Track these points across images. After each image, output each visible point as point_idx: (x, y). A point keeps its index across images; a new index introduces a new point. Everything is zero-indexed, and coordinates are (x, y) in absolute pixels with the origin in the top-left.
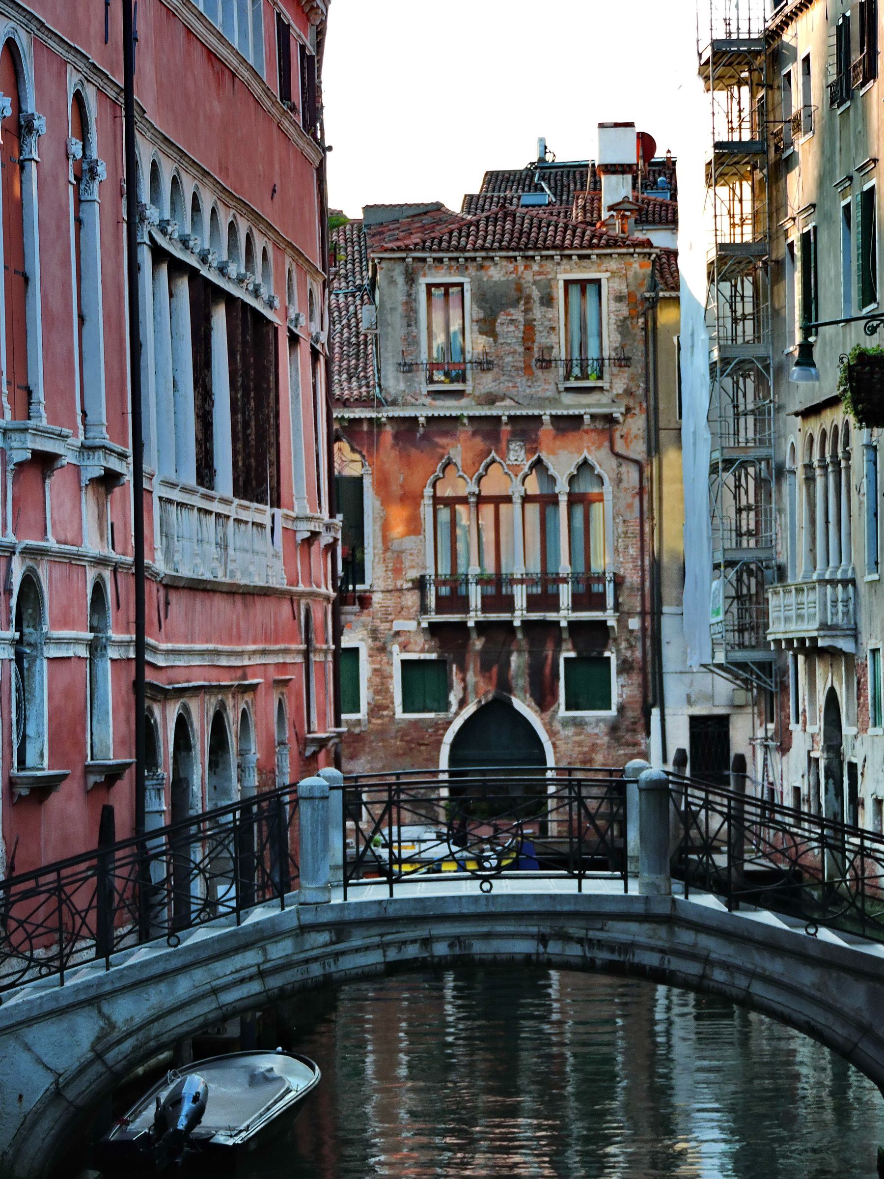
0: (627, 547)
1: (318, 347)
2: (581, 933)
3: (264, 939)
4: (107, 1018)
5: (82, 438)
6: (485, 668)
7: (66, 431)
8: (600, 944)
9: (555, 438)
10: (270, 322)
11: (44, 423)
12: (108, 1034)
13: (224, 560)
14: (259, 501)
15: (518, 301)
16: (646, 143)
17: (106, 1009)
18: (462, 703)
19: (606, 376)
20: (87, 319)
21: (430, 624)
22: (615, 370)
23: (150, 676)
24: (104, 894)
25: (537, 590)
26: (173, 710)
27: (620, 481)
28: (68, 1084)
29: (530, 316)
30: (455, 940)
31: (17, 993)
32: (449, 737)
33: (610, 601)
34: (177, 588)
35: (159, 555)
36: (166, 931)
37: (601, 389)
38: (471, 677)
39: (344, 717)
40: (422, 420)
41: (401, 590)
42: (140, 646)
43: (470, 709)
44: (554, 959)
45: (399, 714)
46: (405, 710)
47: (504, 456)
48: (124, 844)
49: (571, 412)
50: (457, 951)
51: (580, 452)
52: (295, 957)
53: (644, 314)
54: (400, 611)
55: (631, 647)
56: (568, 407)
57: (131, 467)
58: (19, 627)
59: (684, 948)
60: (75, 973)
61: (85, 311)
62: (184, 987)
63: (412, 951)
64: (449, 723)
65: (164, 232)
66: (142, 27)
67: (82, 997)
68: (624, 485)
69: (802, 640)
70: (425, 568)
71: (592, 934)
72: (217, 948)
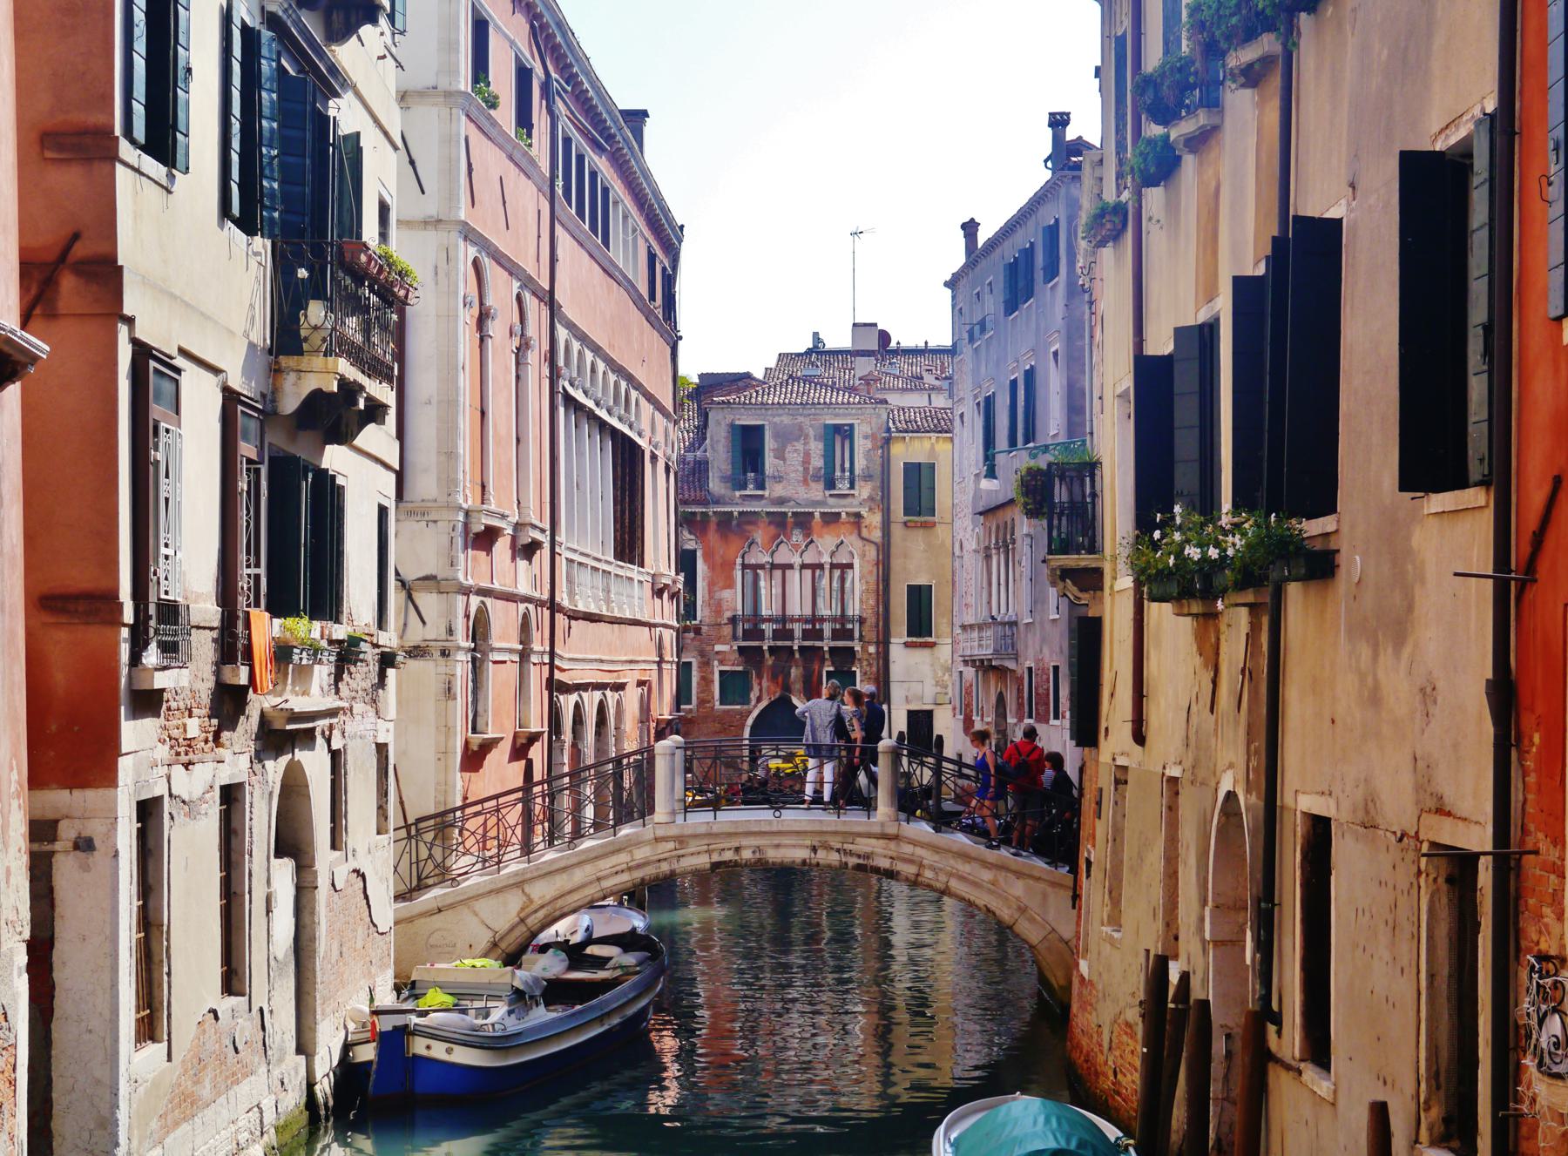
0: (868, 599)
1: (670, 464)
2: (839, 846)
3: (631, 845)
4: (528, 896)
5: (517, 518)
6: (774, 678)
7: (507, 513)
8: (851, 853)
9: (822, 527)
10: (639, 446)
11: (493, 507)
12: (527, 907)
13: (608, 601)
14: (630, 563)
15: (800, 437)
16: (884, 337)
17: (527, 889)
18: (759, 700)
19: (857, 487)
20: (521, 440)
21: (739, 647)
22: (862, 483)
23: (558, 675)
24: (527, 815)
25: (809, 626)
26: (574, 698)
27: (864, 556)
28: (502, 939)
29: (807, 447)
30: (758, 849)
31: (468, 879)
32: (750, 721)
33: (857, 635)
34: (576, 619)
35: (565, 596)
36: (567, 840)
37: (853, 495)
38: (765, 683)
39: (682, 707)
40: (736, 514)
41: (720, 625)
42: (552, 654)
43: (764, 704)
44: (821, 862)
45: (717, 706)
46: (721, 704)
47: (789, 539)
48: (541, 783)
49: (833, 510)
50: (758, 856)
51: (838, 536)
52: (652, 858)
53: (882, 447)
54: (719, 640)
55: (870, 665)
56: (832, 507)
57: (548, 538)
58: (474, 640)
59: (907, 856)
60: (507, 866)
61: (520, 436)
62: (579, 876)
63: (728, 856)
64: (751, 712)
65: (572, 385)
66: (560, 252)
67: (512, 881)
68: (867, 558)
69: (982, 661)
70: (736, 610)
71: (846, 846)
72: (601, 852)
